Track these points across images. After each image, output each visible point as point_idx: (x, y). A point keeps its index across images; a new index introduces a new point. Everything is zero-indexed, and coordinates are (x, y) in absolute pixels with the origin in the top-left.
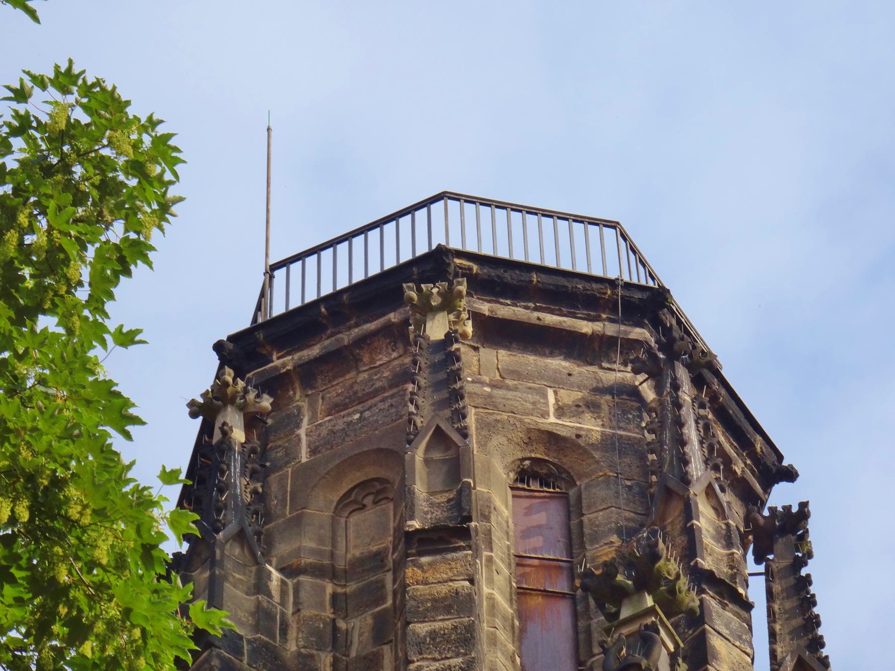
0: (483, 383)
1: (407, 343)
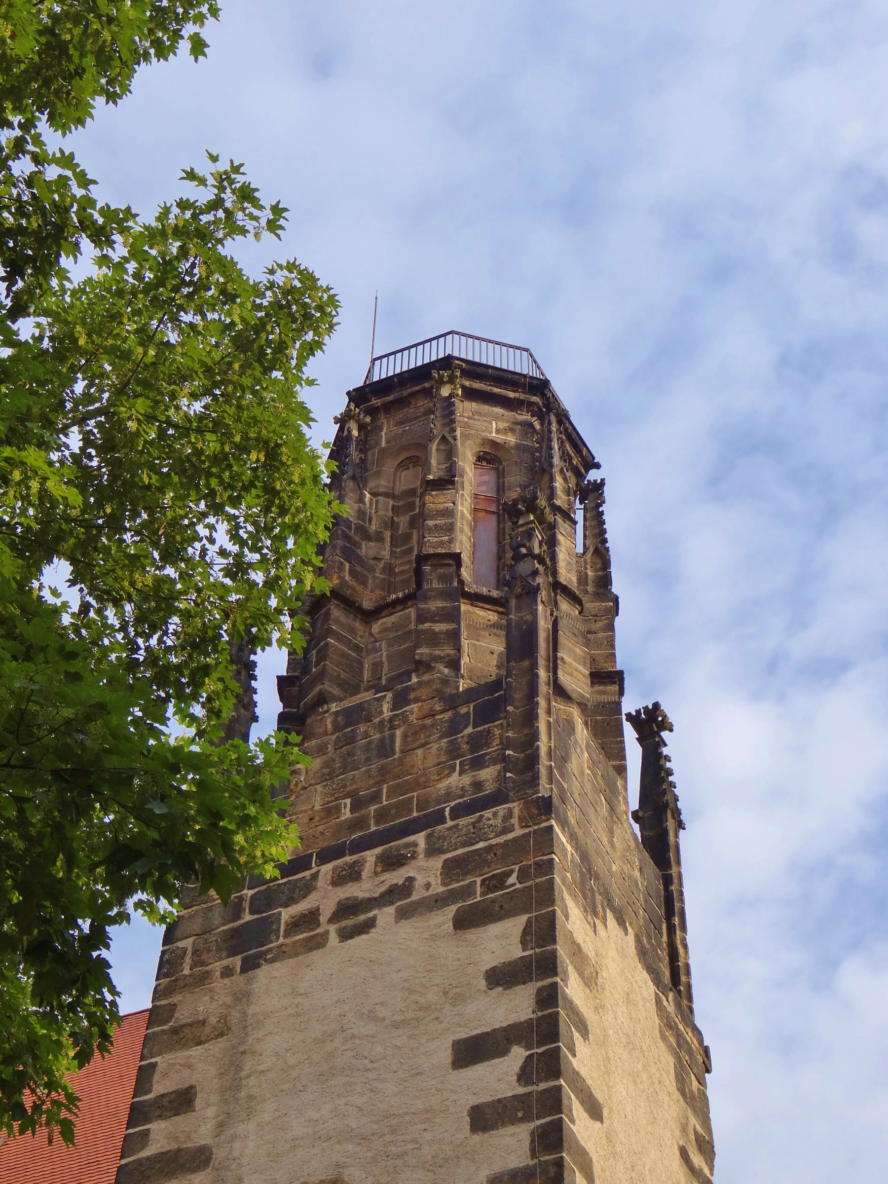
0: (464, 417)
1: (432, 397)
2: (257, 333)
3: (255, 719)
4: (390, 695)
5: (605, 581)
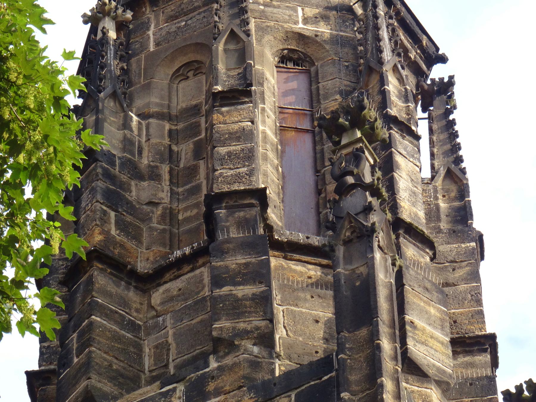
4: (181, 388)
5: (463, 215)
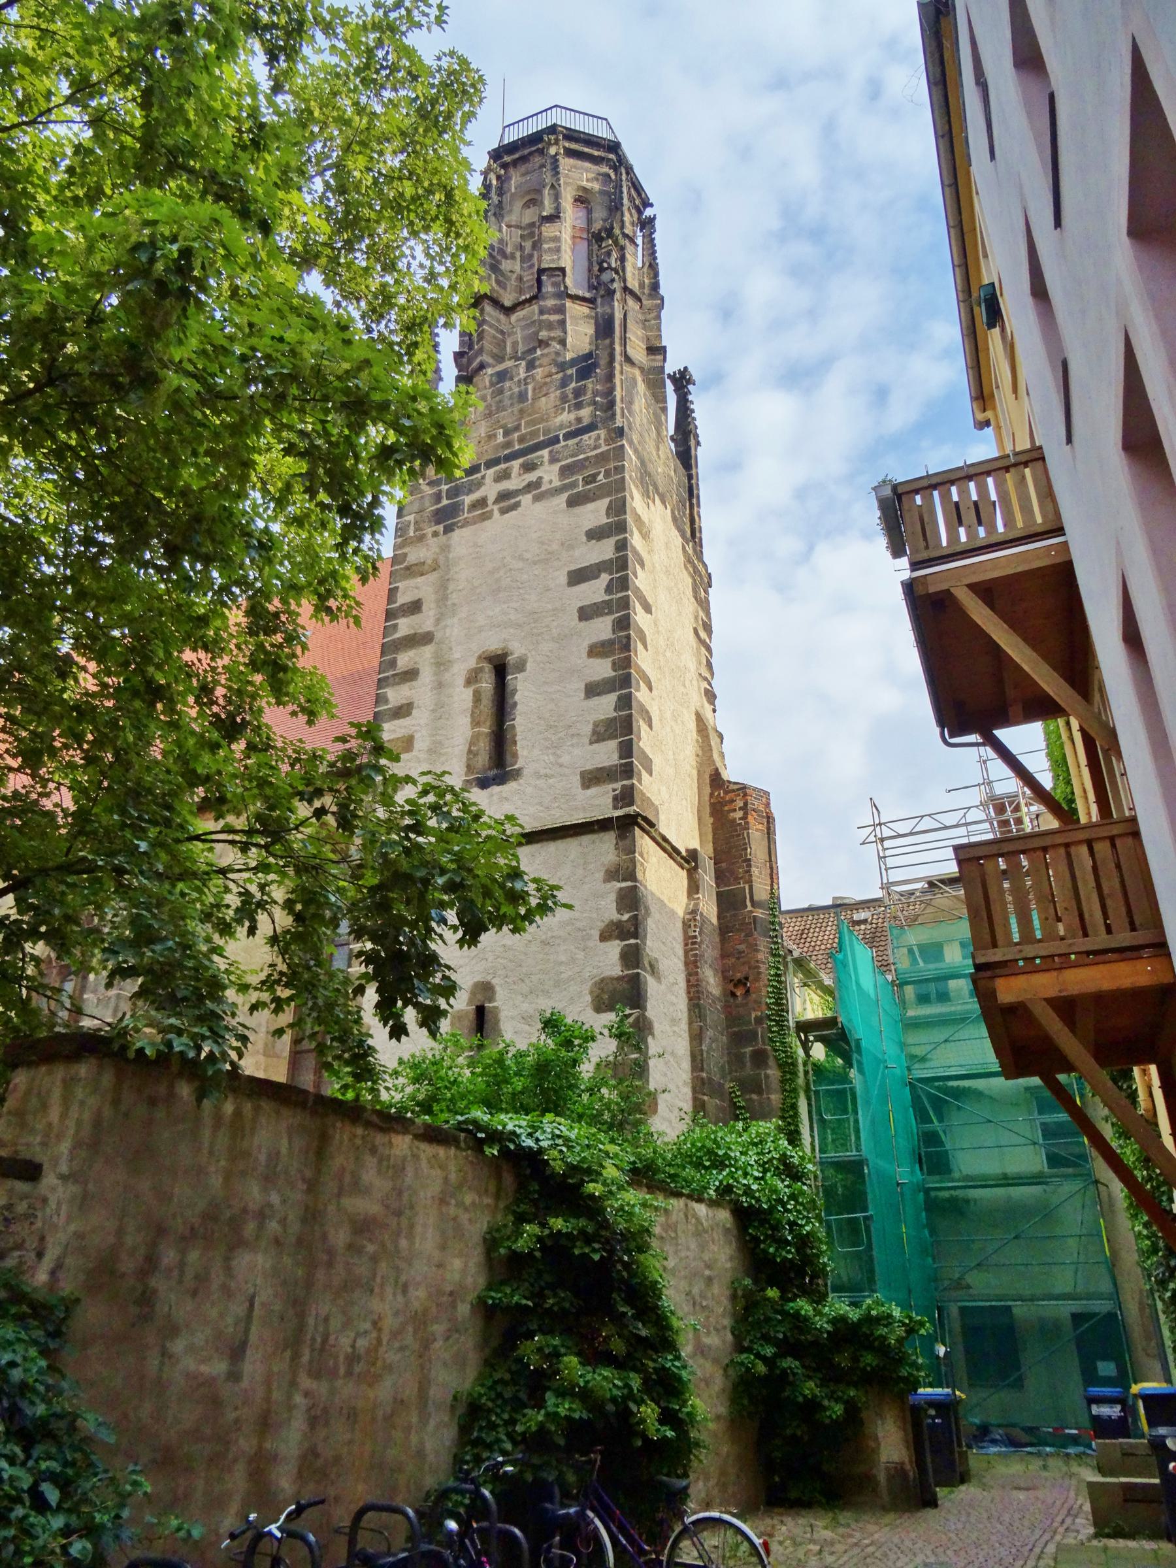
2: (433, 106)
3: (441, 379)
4: (524, 363)
5: (655, 286)
